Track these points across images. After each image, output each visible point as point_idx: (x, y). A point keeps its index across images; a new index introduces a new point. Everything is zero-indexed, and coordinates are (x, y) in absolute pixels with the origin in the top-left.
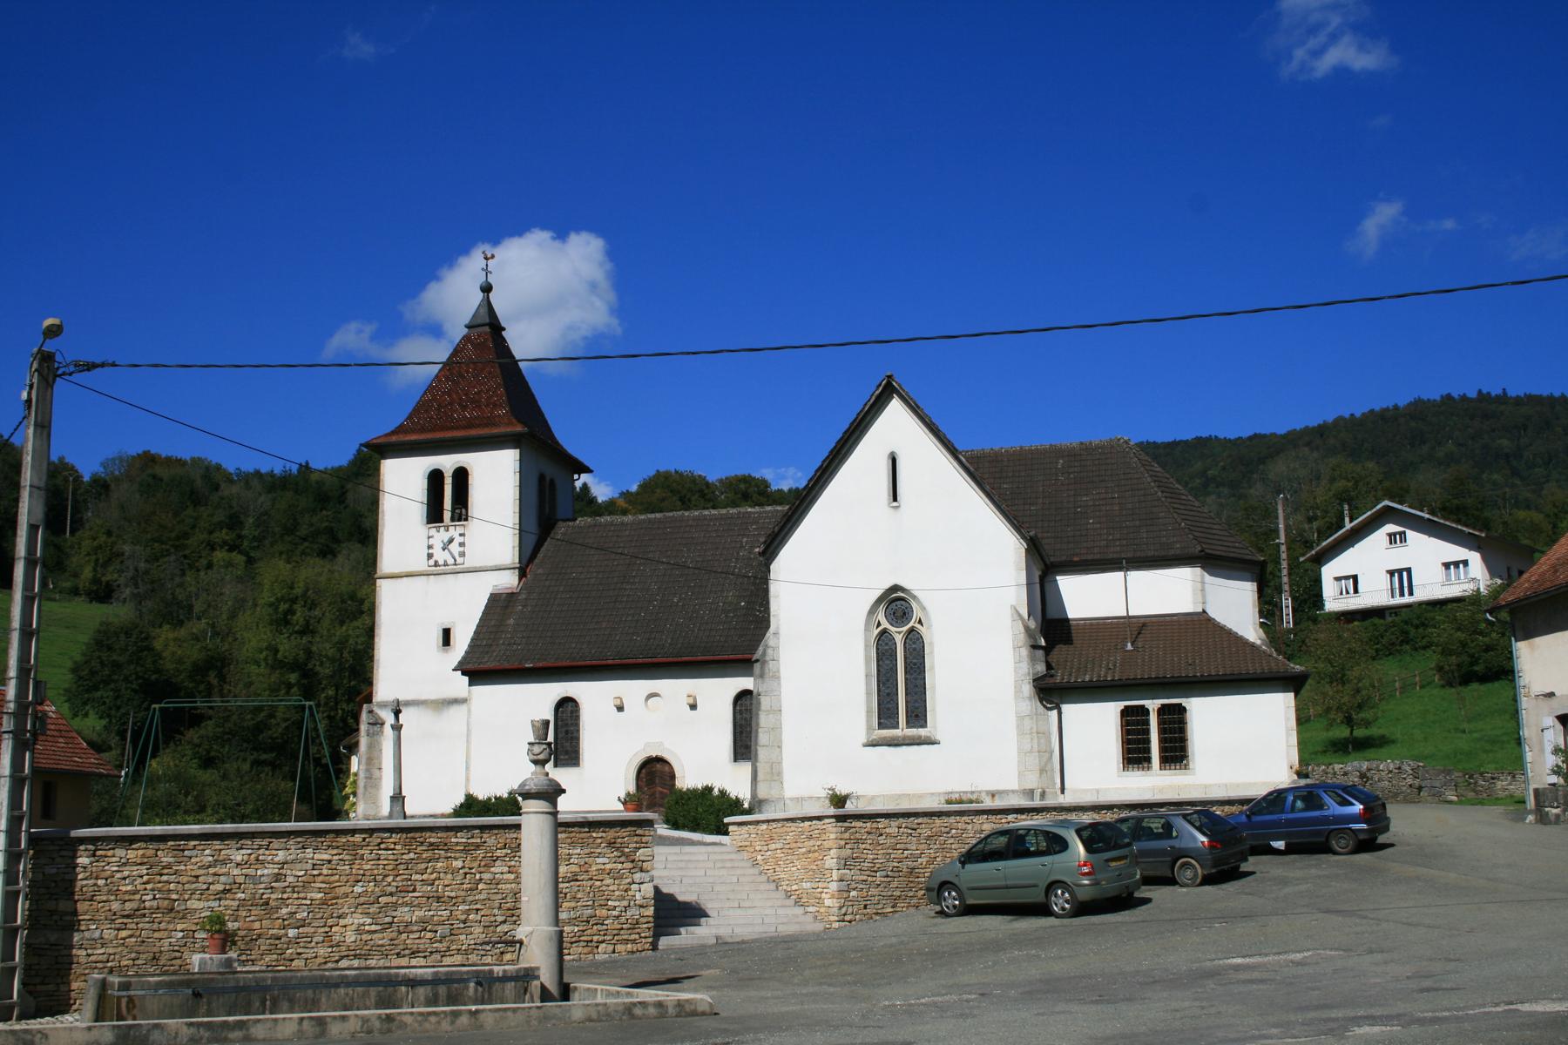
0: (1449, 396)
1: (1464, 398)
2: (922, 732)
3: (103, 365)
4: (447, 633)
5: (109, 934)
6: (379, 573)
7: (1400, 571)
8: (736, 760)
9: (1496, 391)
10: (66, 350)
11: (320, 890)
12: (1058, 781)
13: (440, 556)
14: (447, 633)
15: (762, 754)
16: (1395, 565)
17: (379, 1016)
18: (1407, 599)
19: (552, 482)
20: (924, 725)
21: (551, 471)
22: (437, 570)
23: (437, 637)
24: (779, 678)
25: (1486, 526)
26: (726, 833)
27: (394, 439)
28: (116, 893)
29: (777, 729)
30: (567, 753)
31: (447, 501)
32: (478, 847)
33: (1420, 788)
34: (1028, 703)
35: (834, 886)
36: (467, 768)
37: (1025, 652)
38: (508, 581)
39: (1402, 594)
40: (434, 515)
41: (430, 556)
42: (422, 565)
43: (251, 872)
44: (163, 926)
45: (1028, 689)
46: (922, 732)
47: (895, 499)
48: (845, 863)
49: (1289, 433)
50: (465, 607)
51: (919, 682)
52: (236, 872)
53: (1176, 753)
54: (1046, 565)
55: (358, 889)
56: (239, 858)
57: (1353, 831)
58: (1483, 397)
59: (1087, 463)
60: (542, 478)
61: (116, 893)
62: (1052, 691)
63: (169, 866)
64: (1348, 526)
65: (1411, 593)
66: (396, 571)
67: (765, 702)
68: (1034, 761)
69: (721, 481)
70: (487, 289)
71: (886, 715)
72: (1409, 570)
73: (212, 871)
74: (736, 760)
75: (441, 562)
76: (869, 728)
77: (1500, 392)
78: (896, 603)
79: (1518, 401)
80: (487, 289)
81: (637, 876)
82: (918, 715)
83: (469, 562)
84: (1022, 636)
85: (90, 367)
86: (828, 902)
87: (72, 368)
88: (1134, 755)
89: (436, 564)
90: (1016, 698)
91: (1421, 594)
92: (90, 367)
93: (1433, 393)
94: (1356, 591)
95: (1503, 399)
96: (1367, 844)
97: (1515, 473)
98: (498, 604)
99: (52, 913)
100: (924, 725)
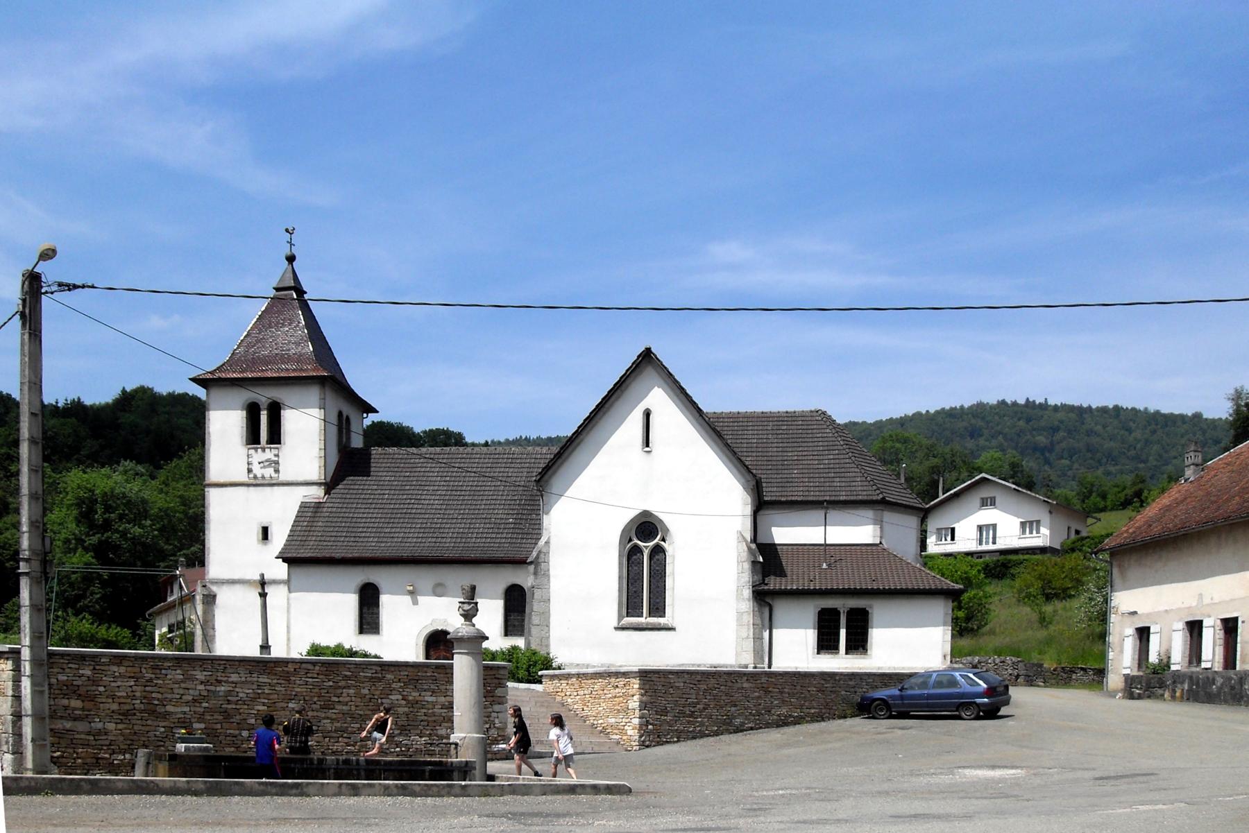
0: (1003, 402)
1: (1015, 404)
2: (661, 621)
3: (83, 287)
4: (265, 532)
5: (111, 726)
6: (207, 482)
7: (988, 526)
8: (506, 635)
9: (1039, 400)
10: (50, 272)
11: (264, 704)
12: (766, 660)
13: (257, 470)
14: (265, 532)
15: (534, 631)
16: (996, 524)
17: (396, 786)
18: (991, 547)
19: (348, 418)
20: (663, 615)
21: (348, 410)
22: (256, 483)
23: (256, 533)
24: (549, 576)
25: (1055, 498)
26: (541, 682)
27: (217, 375)
28: (113, 697)
29: (546, 615)
30: (368, 624)
31: (264, 428)
32: (380, 680)
33: (1018, 677)
34: (747, 605)
35: (636, 721)
36: (288, 632)
37: (747, 566)
38: (317, 493)
39: (987, 543)
40: (253, 438)
41: (250, 471)
42: (243, 477)
43: (212, 688)
44: (149, 722)
45: (747, 593)
46: (661, 621)
47: (648, 446)
48: (644, 705)
49: (877, 422)
50: (282, 509)
51: (661, 584)
52: (202, 687)
53: (858, 643)
54: (762, 505)
55: (291, 705)
56: (203, 678)
57: (978, 705)
58: (1029, 404)
59: (808, 428)
60: (340, 414)
61: (113, 697)
62: (764, 597)
63: (151, 680)
64: (941, 497)
65: (994, 543)
66: (222, 480)
67: (538, 594)
68: (749, 644)
69: (425, 432)
70: (291, 259)
71: (631, 605)
72: (994, 526)
73: (183, 685)
74: (506, 635)
75: (259, 475)
76: (620, 618)
77: (1042, 401)
78: (646, 527)
79: (1056, 408)
80: (291, 259)
81: (497, 708)
82: (658, 608)
83: (283, 477)
84: (745, 554)
85: (72, 287)
86: (629, 733)
87: (55, 288)
88: (826, 643)
89: (255, 477)
90: (738, 599)
91: (1002, 544)
92: (72, 287)
93: (992, 399)
94: (953, 539)
95: (1044, 407)
96: (991, 713)
97: (1047, 462)
98: (308, 512)
99: (66, 708)
100: (663, 615)
